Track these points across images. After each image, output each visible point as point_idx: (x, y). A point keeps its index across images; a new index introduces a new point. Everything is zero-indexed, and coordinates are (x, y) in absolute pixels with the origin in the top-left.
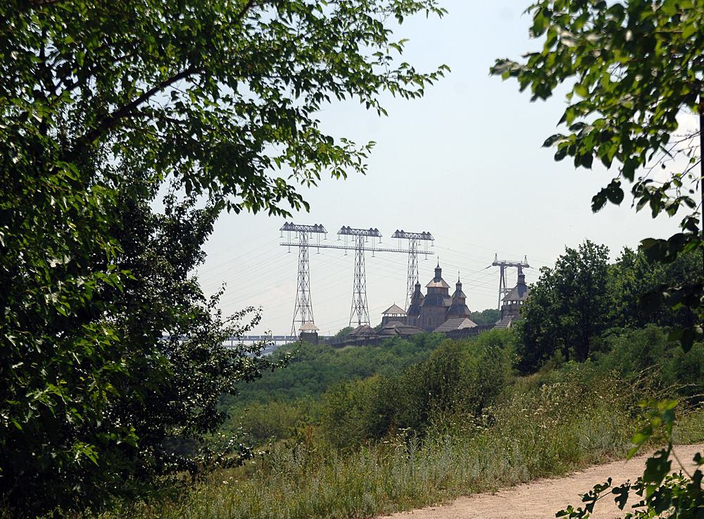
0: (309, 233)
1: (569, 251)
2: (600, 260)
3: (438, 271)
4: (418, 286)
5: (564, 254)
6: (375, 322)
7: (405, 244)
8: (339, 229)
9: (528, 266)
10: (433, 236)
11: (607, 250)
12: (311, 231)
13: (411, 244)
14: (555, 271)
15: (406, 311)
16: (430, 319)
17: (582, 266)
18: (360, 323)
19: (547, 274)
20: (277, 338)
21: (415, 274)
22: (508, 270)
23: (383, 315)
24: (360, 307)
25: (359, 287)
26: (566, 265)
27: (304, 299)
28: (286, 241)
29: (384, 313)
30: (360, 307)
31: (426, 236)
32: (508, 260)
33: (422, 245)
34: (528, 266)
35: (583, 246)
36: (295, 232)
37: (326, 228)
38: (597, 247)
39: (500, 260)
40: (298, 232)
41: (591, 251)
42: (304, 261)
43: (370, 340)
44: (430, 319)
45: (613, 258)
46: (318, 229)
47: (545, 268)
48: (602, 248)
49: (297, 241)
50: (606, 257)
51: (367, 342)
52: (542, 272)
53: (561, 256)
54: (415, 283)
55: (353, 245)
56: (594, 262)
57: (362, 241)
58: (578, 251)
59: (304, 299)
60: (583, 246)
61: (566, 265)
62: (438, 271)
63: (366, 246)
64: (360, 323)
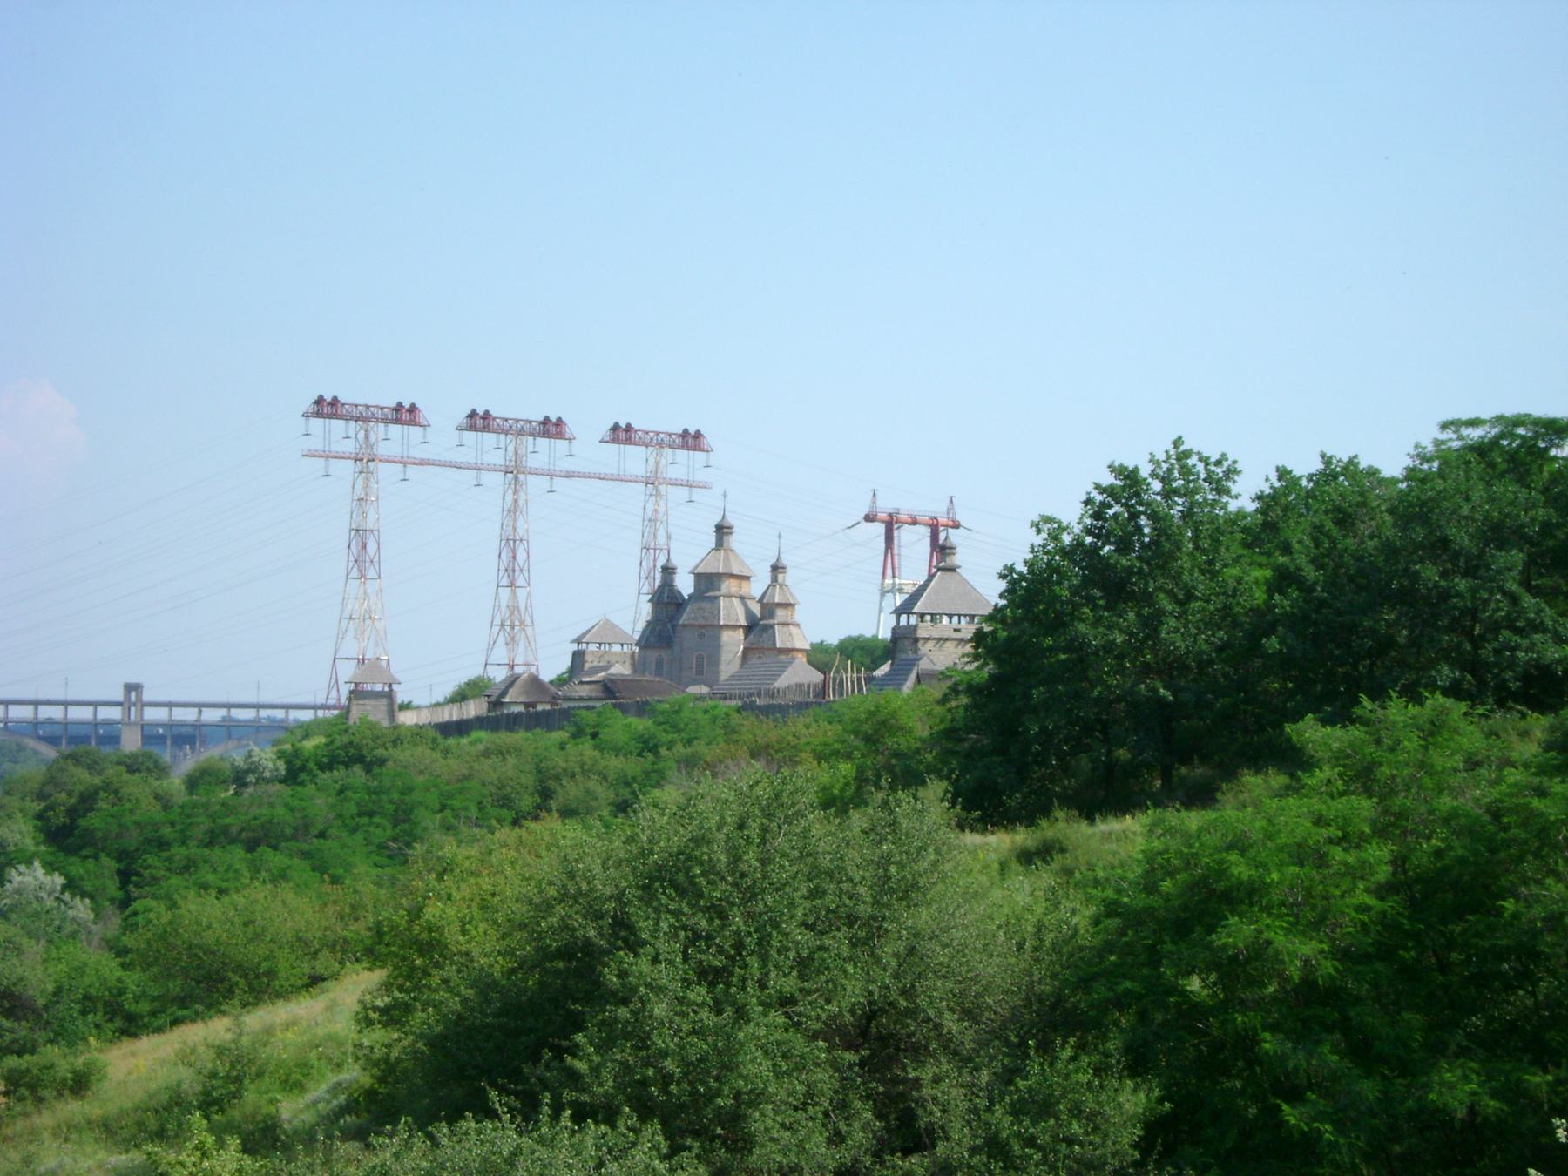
0: (381, 426)
1: (1119, 471)
2: (1210, 497)
3: (722, 530)
4: (668, 571)
5: (1108, 479)
6: (552, 666)
7: (635, 459)
8: (307, 404)
9: (956, 526)
10: (710, 439)
11: (1231, 473)
12: (385, 421)
13: (652, 461)
14: (1077, 529)
15: (637, 636)
16: (700, 658)
17: (1154, 517)
18: (512, 667)
19: (1054, 537)
20: (791, 594)
21: (661, 540)
22: (904, 535)
23: (575, 647)
24: (512, 624)
25: (511, 571)
26: (1111, 512)
27: (514, 609)
28: (316, 444)
29: (578, 641)
30: (512, 624)
31: (691, 440)
32: (906, 505)
33: (681, 463)
34: (956, 526)
35: (1162, 457)
36: (342, 422)
37: (426, 413)
38: (1205, 460)
39: (885, 505)
40: (352, 423)
41: (1186, 471)
42: (514, 510)
43: (537, 714)
44: (700, 658)
45: (1244, 497)
46: (406, 416)
47: (1048, 520)
48: (1218, 463)
49: (349, 447)
50: (1227, 492)
51: (533, 720)
52: (1039, 531)
53: (1097, 487)
54: (661, 561)
55: (498, 459)
56: (1193, 504)
57: (372, 437)
58: (1145, 472)
59: (514, 609)
60: (1162, 457)
61: (1111, 512)
62: (722, 530)
63: (532, 462)
64: (512, 667)
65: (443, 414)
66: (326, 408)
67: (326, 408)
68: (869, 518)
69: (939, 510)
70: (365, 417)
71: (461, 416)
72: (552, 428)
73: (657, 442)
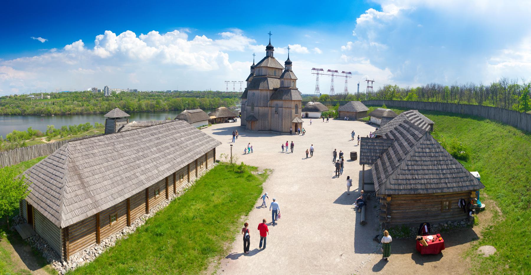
7: (345, 75)
10: (352, 73)
22: (369, 82)
27: (346, 89)
28: (313, 73)
32: (370, 80)
39: (368, 79)
49: (316, 73)
55: (331, 74)
65: (340, 72)
66: (314, 69)
67: (314, 69)
68: (366, 80)
69: (373, 80)
70: (318, 70)
71: (342, 72)
72: (336, 71)
73: (333, 71)
